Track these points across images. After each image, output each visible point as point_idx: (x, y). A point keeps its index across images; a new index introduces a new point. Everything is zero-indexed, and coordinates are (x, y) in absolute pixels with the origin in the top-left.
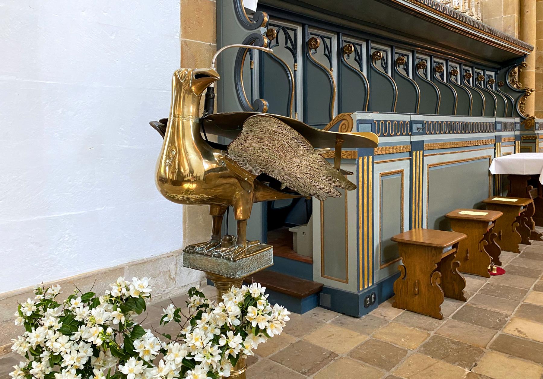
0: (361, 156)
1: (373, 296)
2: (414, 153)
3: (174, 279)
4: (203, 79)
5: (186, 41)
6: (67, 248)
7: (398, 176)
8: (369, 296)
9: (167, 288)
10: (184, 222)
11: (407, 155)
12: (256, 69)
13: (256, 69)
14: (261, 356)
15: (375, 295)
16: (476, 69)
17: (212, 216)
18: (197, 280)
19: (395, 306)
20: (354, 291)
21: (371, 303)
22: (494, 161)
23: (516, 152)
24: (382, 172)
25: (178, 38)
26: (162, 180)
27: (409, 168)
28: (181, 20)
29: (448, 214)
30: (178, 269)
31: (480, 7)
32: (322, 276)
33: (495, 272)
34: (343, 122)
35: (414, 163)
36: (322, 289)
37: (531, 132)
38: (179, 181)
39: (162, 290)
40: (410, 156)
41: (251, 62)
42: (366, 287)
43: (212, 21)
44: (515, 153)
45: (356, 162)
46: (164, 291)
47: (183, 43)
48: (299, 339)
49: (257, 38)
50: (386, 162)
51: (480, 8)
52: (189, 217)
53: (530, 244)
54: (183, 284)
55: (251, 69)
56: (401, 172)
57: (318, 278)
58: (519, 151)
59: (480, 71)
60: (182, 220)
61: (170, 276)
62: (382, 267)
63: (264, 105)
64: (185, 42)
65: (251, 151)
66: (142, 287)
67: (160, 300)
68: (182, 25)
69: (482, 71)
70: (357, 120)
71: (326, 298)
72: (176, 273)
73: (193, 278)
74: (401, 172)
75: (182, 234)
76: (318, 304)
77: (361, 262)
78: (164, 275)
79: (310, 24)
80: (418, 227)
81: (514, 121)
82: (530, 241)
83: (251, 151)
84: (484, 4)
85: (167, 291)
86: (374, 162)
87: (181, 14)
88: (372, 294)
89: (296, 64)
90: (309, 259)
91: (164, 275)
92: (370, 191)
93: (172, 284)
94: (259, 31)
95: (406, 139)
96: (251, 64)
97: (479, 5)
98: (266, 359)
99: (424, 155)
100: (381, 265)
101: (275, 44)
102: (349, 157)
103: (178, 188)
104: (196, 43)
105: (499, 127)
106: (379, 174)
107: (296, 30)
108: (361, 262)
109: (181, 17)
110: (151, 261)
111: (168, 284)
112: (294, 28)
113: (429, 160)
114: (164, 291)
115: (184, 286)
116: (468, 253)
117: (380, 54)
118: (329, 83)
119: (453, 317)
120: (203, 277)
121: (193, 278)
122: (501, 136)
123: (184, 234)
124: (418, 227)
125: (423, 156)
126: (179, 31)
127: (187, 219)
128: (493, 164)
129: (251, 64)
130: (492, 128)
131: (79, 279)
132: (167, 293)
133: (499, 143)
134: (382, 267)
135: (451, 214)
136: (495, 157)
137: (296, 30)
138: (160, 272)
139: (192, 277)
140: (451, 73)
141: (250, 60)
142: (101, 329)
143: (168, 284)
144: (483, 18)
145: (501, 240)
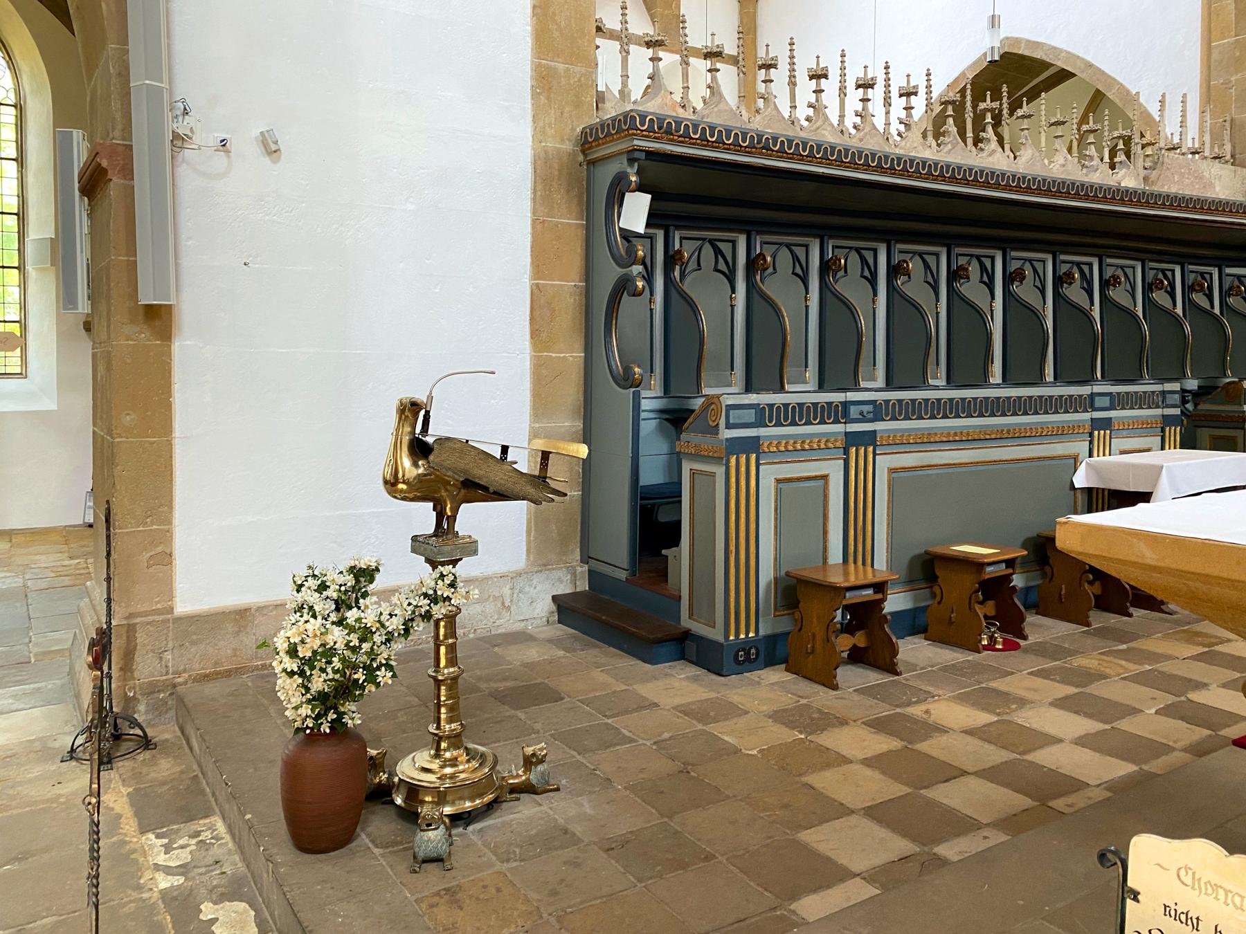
0: (734, 454)
1: (753, 651)
2: (1168, 429)
3: (509, 608)
4: (415, 407)
5: (538, 284)
6: (373, 552)
7: (821, 482)
8: (743, 650)
9: (498, 619)
10: (529, 532)
11: (840, 453)
12: (658, 309)
13: (658, 309)
14: (569, 697)
15: (757, 649)
16: (1190, 267)
17: (435, 513)
18: (543, 615)
19: (787, 670)
20: (720, 638)
21: (748, 659)
22: (1084, 463)
23: (1167, 447)
24: (781, 476)
25: (527, 281)
26: (386, 482)
27: (842, 473)
28: (531, 255)
29: (931, 549)
30: (515, 595)
31: (1229, 129)
32: (690, 618)
33: (1000, 647)
34: (713, 406)
35: (853, 464)
36: (686, 635)
37: (1235, 408)
38: (395, 484)
39: (492, 621)
40: (845, 454)
41: (650, 299)
42: (742, 636)
43: (579, 251)
44: (1163, 448)
45: (724, 462)
46: (494, 622)
47: (534, 287)
48: (627, 687)
49: (628, 280)
50: (787, 462)
51: (1229, 132)
52: (536, 524)
53: (1130, 615)
54: (522, 618)
55: (651, 310)
56: (825, 478)
57: (686, 622)
58: (1178, 446)
59: (1212, 268)
60: (525, 528)
61: (503, 603)
62: (777, 613)
63: (635, 374)
64: (537, 285)
65: (448, 462)
66: (370, 561)
67: (489, 634)
68: (532, 263)
69: (1217, 269)
70: (727, 406)
71: (691, 647)
72: (511, 601)
73: (537, 611)
74: (825, 478)
75: (525, 549)
76: (682, 656)
77: (732, 600)
78: (494, 601)
79: (759, 229)
80: (864, 564)
81: (1161, 389)
82: (1132, 610)
83: (448, 462)
84: (1238, 123)
85: (498, 623)
86: (877, 452)
87: (532, 247)
88: (751, 648)
89: (733, 295)
90: (676, 593)
91: (494, 601)
92: (753, 503)
93: (506, 614)
94: (631, 271)
95: (839, 428)
96: (650, 303)
97: (1228, 125)
98: (574, 700)
99: (877, 452)
100: (776, 610)
101: (696, 266)
102: (715, 455)
103: (394, 488)
104: (552, 285)
105: (1099, 402)
106: (773, 480)
107: (735, 241)
108: (732, 600)
109: (532, 251)
110: (477, 580)
111: (499, 613)
112: (730, 238)
113: (884, 463)
114: (494, 622)
115: (523, 620)
116: (952, 612)
117: (908, 266)
118: (779, 326)
119: (855, 691)
120: (553, 612)
121: (537, 611)
122: (1111, 418)
123: (527, 550)
124: (864, 564)
125: (875, 454)
126: (528, 272)
127: (533, 529)
128: (1082, 469)
129: (650, 303)
130: (1089, 403)
131: (384, 592)
132: (498, 626)
133: (1102, 432)
134: (777, 613)
135: (940, 550)
136: (1091, 455)
137: (735, 241)
138: (489, 597)
139: (535, 608)
140: (1108, 282)
141: (649, 297)
142: (337, 587)
143: (499, 613)
144: (1237, 152)
145: (1062, 602)
